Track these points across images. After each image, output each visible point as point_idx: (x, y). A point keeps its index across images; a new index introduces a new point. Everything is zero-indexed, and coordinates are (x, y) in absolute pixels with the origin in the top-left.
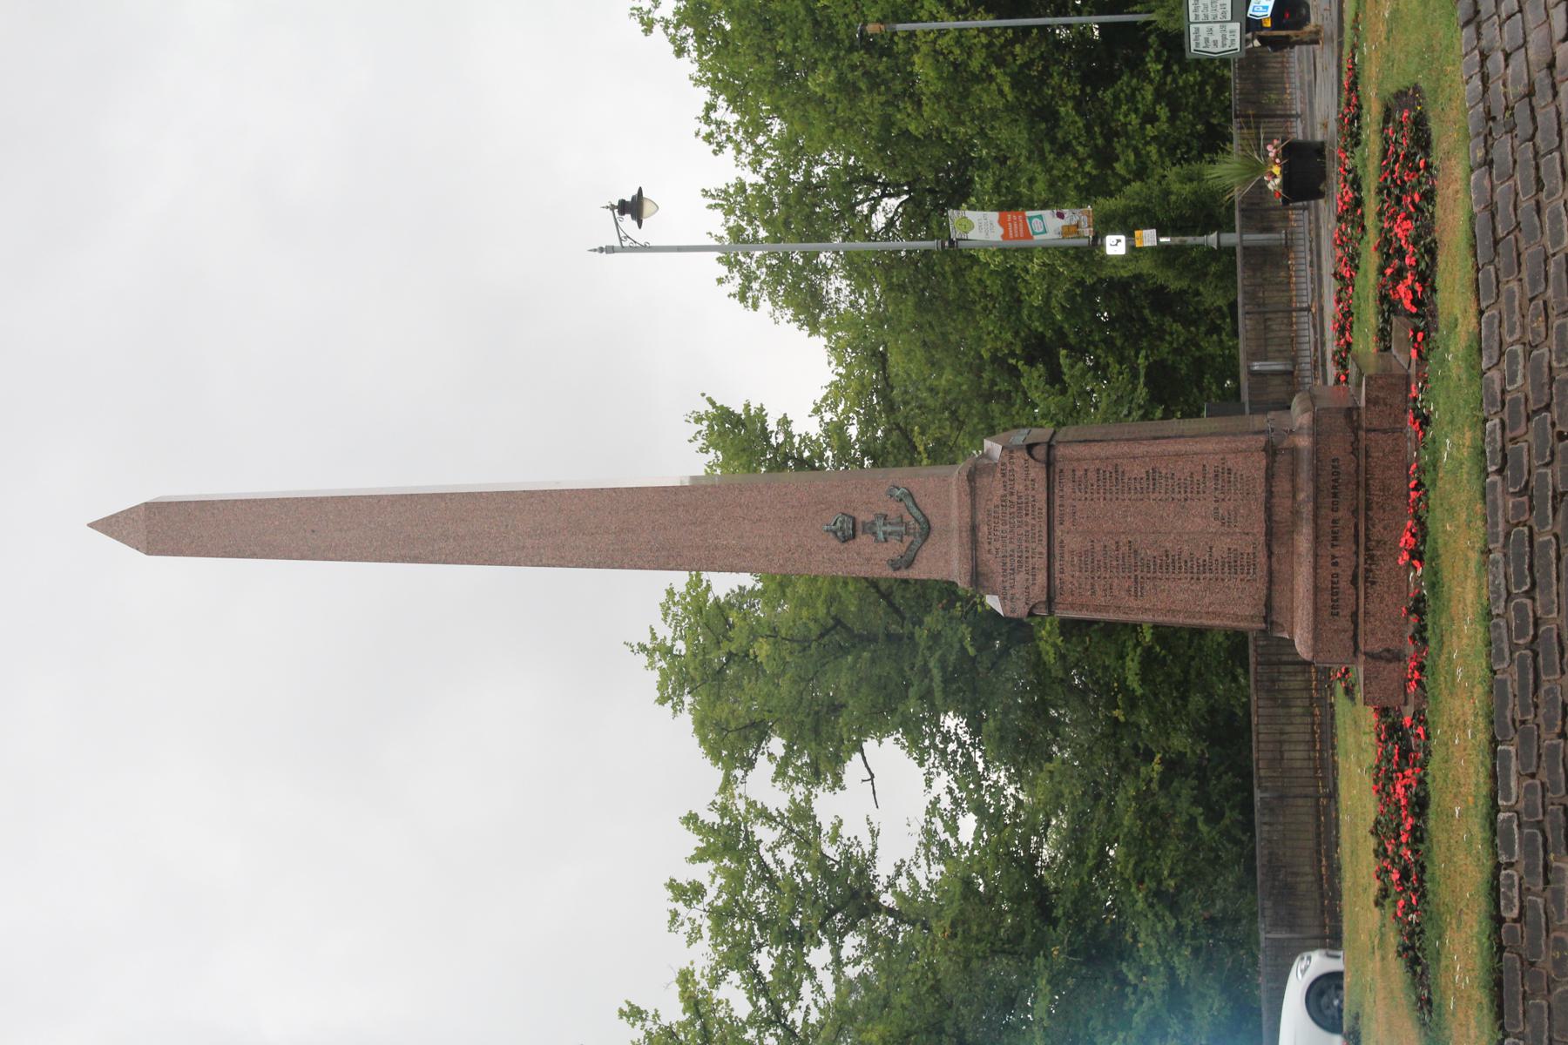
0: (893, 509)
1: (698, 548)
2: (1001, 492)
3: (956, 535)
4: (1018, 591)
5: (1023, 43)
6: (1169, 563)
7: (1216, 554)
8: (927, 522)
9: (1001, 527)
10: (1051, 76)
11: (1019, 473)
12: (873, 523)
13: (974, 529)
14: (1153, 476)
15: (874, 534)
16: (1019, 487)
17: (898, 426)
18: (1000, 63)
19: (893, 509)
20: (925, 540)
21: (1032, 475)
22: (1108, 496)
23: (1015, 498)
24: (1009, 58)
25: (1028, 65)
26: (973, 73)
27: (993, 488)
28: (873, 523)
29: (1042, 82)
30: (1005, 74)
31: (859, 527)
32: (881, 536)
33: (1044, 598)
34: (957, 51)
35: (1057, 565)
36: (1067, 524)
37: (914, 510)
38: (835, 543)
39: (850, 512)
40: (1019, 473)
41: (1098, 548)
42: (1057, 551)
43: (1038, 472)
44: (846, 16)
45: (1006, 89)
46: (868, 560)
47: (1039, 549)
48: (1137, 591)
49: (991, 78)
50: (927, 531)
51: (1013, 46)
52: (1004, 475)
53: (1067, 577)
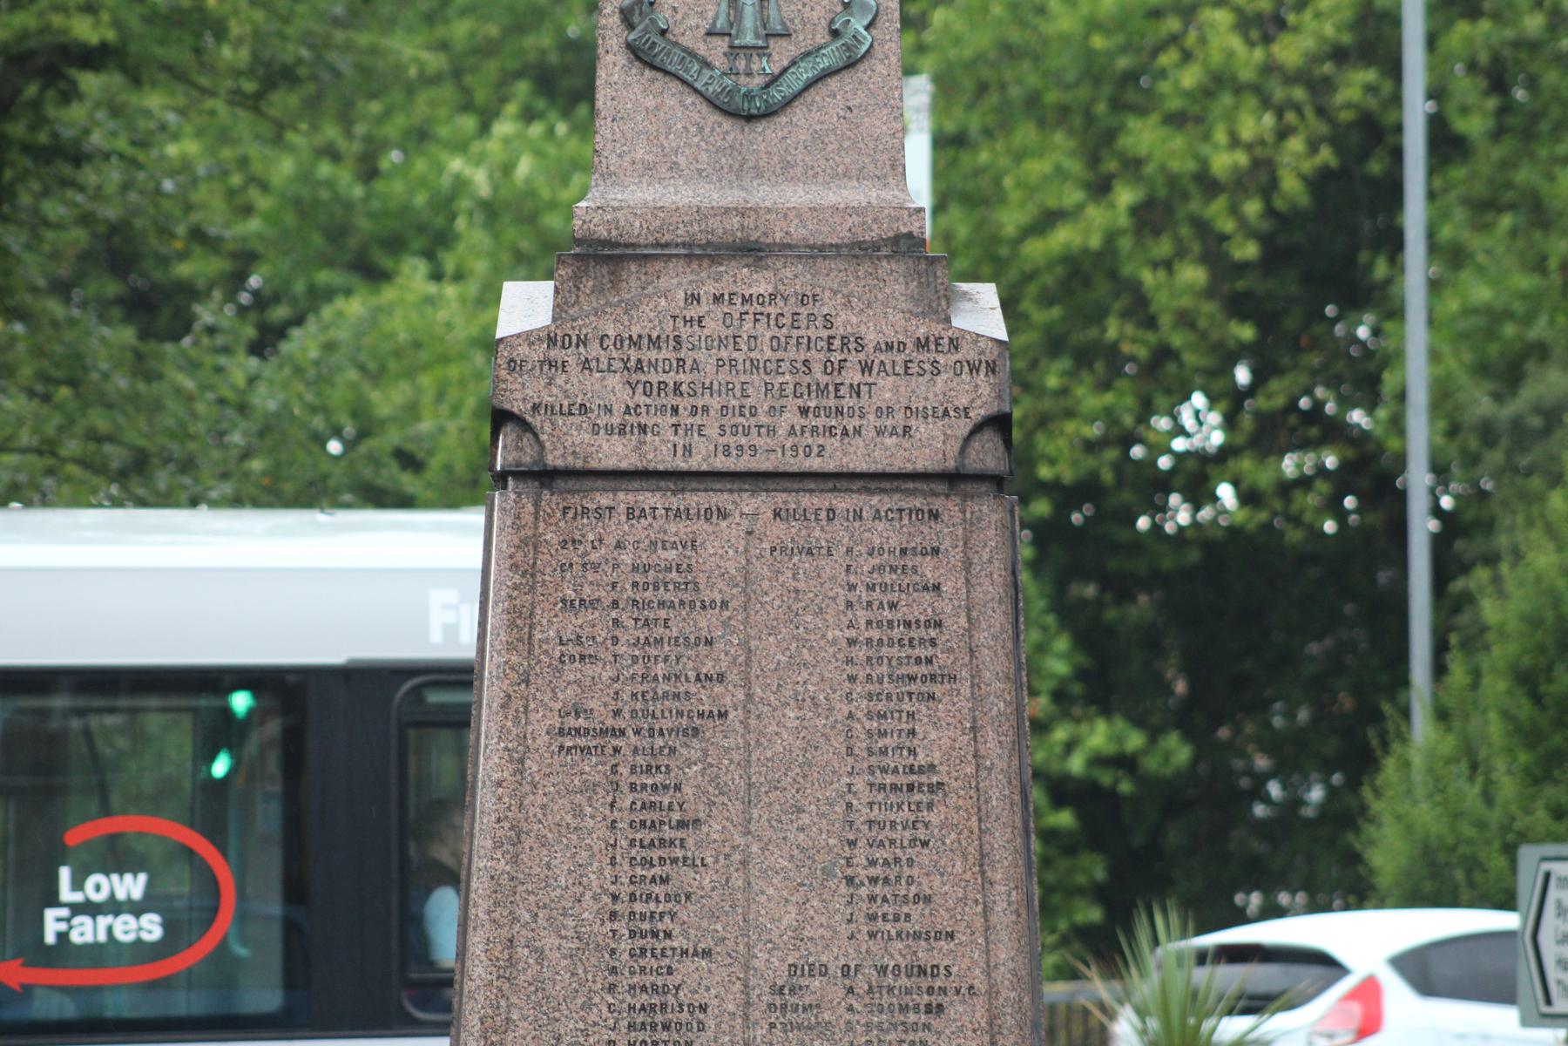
2: (871, 338)
3: (732, 196)
4: (575, 383)
5: (1210, 292)
6: (659, 833)
7: (688, 970)
8: (769, 114)
9: (766, 333)
10: (1105, 386)
11: (928, 392)
13: (752, 251)
14: (920, 784)
16: (886, 389)
18: (1150, 218)
20: (710, 102)
21: (922, 429)
22: (861, 653)
23: (853, 376)
25: (1141, 310)
26: (1110, 136)
27: (879, 311)
29: (1084, 357)
30: (1111, 237)
33: (554, 459)
34: (1190, 78)
35: (650, 499)
36: (778, 530)
37: (805, 73)
40: (928, 392)
41: (707, 622)
42: (696, 499)
43: (932, 446)
45: (1063, 237)
47: (702, 448)
48: (579, 736)
49: (1101, 188)
50: (745, 112)
52: (922, 344)
53: (617, 527)
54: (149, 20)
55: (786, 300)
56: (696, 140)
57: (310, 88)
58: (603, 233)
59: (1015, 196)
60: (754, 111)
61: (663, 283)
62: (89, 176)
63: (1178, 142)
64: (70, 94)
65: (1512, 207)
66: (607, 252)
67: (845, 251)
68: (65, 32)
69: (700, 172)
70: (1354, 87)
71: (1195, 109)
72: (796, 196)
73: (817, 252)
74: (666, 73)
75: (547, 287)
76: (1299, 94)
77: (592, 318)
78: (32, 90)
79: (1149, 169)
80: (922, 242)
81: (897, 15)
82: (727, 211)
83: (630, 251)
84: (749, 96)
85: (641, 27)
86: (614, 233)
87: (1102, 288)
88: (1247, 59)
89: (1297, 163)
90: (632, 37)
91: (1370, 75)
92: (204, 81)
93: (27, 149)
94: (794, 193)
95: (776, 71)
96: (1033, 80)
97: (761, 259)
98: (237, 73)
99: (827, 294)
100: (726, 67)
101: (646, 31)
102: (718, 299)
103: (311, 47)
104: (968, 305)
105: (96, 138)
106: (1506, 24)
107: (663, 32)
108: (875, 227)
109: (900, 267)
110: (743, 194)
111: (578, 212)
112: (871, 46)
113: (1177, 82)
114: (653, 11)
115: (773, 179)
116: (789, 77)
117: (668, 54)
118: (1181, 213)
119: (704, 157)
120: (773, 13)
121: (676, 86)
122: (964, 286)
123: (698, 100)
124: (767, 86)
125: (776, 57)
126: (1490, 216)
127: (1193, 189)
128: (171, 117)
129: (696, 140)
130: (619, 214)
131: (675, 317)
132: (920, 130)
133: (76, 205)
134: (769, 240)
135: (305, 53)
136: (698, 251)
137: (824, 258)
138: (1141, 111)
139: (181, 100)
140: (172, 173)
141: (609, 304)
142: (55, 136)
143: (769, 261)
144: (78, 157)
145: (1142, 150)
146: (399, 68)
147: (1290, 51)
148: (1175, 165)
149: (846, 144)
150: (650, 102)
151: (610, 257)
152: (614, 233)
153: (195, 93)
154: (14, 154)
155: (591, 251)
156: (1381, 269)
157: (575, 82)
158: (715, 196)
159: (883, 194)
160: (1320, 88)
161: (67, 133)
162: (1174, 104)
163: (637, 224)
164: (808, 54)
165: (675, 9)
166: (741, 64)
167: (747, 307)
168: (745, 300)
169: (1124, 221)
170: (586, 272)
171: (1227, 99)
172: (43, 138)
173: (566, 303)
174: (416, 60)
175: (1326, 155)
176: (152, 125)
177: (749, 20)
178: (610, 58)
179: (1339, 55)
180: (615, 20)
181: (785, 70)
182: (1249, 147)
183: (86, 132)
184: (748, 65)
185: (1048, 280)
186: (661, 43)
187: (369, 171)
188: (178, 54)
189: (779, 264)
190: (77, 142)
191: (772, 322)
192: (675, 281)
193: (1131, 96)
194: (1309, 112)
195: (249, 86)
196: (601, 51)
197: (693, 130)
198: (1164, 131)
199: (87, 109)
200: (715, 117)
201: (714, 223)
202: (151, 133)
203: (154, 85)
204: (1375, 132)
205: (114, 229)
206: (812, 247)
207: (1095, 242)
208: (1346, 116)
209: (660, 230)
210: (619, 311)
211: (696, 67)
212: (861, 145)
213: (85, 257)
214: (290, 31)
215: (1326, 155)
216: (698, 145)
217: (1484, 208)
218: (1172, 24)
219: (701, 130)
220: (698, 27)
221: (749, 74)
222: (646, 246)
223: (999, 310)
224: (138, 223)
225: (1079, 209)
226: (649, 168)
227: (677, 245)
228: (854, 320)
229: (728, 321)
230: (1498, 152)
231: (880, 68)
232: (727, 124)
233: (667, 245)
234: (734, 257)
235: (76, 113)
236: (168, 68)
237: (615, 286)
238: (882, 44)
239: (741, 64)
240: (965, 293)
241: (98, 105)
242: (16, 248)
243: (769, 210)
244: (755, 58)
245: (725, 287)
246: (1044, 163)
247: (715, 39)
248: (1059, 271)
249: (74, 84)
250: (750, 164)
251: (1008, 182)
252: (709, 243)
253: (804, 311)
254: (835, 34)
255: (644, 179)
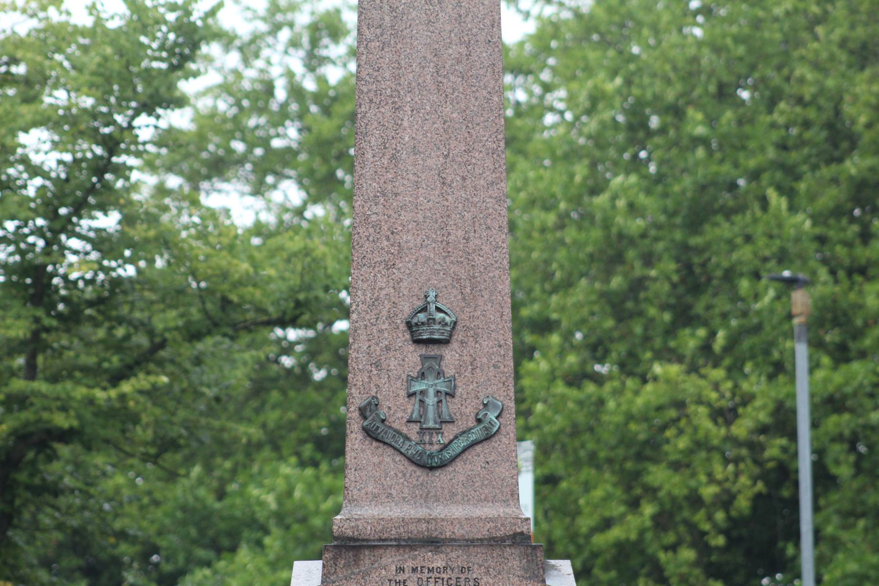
0: (463, 409)
1: (396, 78)
3: (422, 512)
5: (696, 564)
8: (442, 466)
12: (439, 374)
13: (433, 543)
15: (422, 375)
17: (163, 345)
18: (661, 522)
19: (463, 409)
20: (410, 460)
24: (670, 538)
26: (637, 475)
28: (439, 374)
30: (642, 532)
31: (434, 350)
32: (418, 387)
34: (683, 443)
37: (462, 443)
38: (406, 309)
39: (459, 336)
44: (748, 239)
45: (616, 533)
46: (377, 365)
49: (634, 505)
50: (429, 465)
51: (693, 545)
54: (96, 415)
55: (453, 570)
56: (402, 481)
57: (186, 451)
58: (349, 533)
59: (587, 510)
60: (434, 465)
61: (384, 561)
62: (62, 501)
63: (677, 479)
64: (53, 457)
65: (863, 515)
66: (352, 544)
67: (485, 542)
68: (48, 422)
69: (404, 498)
70: (774, 448)
71: (686, 460)
72: (457, 511)
73: (469, 543)
74: (385, 443)
75: (318, 564)
76: (744, 452)
77: (344, 581)
78: (31, 455)
79: (661, 494)
80: (529, 537)
81: (513, 410)
82: (419, 520)
83: (365, 543)
84: (431, 456)
85: (370, 418)
86: (356, 533)
87: (635, 562)
88: (716, 433)
89: (747, 489)
90: (365, 424)
91: (783, 441)
92: (127, 448)
93: (29, 487)
94: (457, 509)
95: (447, 442)
96: (591, 446)
97: (438, 547)
98: (146, 444)
99: (476, 566)
100: (418, 440)
101: (373, 420)
102: (414, 570)
103: (187, 428)
104: (555, 573)
105: (68, 481)
106: (860, 416)
107: (383, 421)
108: (502, 529)
109: (516, 551)
110: (428, 511)
111: (336, 522)
112: (499, 428)
113: (676, 445)
114: (377, 409)
115: (445, 502)
116: (453, 445)
117: (386, 433)
118: (678, 519)
119: (406, 490)
120: (444, 409)
121: (390, 451)
122: (553, 562)
123: (403, 458)
124: (441, 450)
125: (446, 434)
126: (851, 520)
127: (685, 504)
128: (109, 468)
129: (402, 481)
130: (359, 523)
131: (390, 581)
132: (528, 471)
133: (55, 518)
134: (443, 537)
135: (183, 432)
136: (403, 543)
137: (474, 546)
138: (655, 461)
139: (114, 459)
140: (109, 500)
141: (353, 573)
142: (44, 480)
143: (443, 549)
144: (56, 491)
145: (656, 484)
146: (236, 440)
147: (741, 429)
148: (676, 492)
149: (486, 482)
150: (376, 460)
151: (354, 547)
152: (356, 533)
153: (122, 455)
154: (20, 491)
155: (343, 543)
156: (790, 551)
157: (335, 445)
158: (413, 512)
159: (507, 510)
160: (755, 448)
161: (50, 478)
162: (674, 457)
163: (369, 528)
164: (464, 432)
165: (389, 408)
166: (427, 438)
167: (430, 575)
168: (430, 570)
169: (648, 523)
170: (340, 555)
171: (703, 454)
172: (37, 481)
173: (329, 573)
174: (246, 434)
175: (760, 486)
176: (98, 473)
177: (431, 413)
178: (353, 435)
179: (763, 429)
180: (356, 415)
181: (451, 441)
182: (719, 483)
183: (61, 478)
184: (430, 439)
185: (608, 556)
186: (382, 427)
187: (221, 495)
188: (112, 433)
189: (448, 550)
190: (56, 483)
191: (445, 583)
192: (390, 560)
193: (648, 452)
194: (749, 462)
195: (152, 451)
196: (348, 432)
197: (400, 475)
198: (669, 472)
199: (60, 468)
200: (412, 468)
201: (412, 527)
202: (97, 477)
203: (98, 450)
204: (785, 473)
205: (76, 532)
206: (467, 540)
207: (633, 536)
208: (771, 465)
209: (381, 531)
210: (359, 577)
211: (402, 440)
212: (494, 483)
213: (60, 546)
214: (175, 419)
215: (760, 486)
216: (403, 484)
217: (850, 516)
218: (673, 413)
219: (404, 475)
220: (402, 418)
221: (431, 444)
222: (374, 541)
223: (573, 575)
224: (90, 528)
225: (623, 516)
226: (376, 496)
227: (391, 540)
228: (491, 581)
229: (420, 582)
230: (856, 485)
231: (504, 440)
232: (419, 472)
233: (385, 540)
234: (423, 546)
235: (56, 467)
236: (107, 441)
237: (357, 562)
238: (505, 426)
239: (427, 438)
240: (553, 566)
241: (67, 462)
242: (21, 543)
243: (443, 520)
244: (435, 435)
245: (418, 563)
246: (602, 491)
247: (412, 424)
248: (613, 551)
249: (54, 451)
250: (432, 494)
251: (582, 502)
252: (409, 538)
253: (463, 576)
254: (479, 421)
255: (372, 503)
